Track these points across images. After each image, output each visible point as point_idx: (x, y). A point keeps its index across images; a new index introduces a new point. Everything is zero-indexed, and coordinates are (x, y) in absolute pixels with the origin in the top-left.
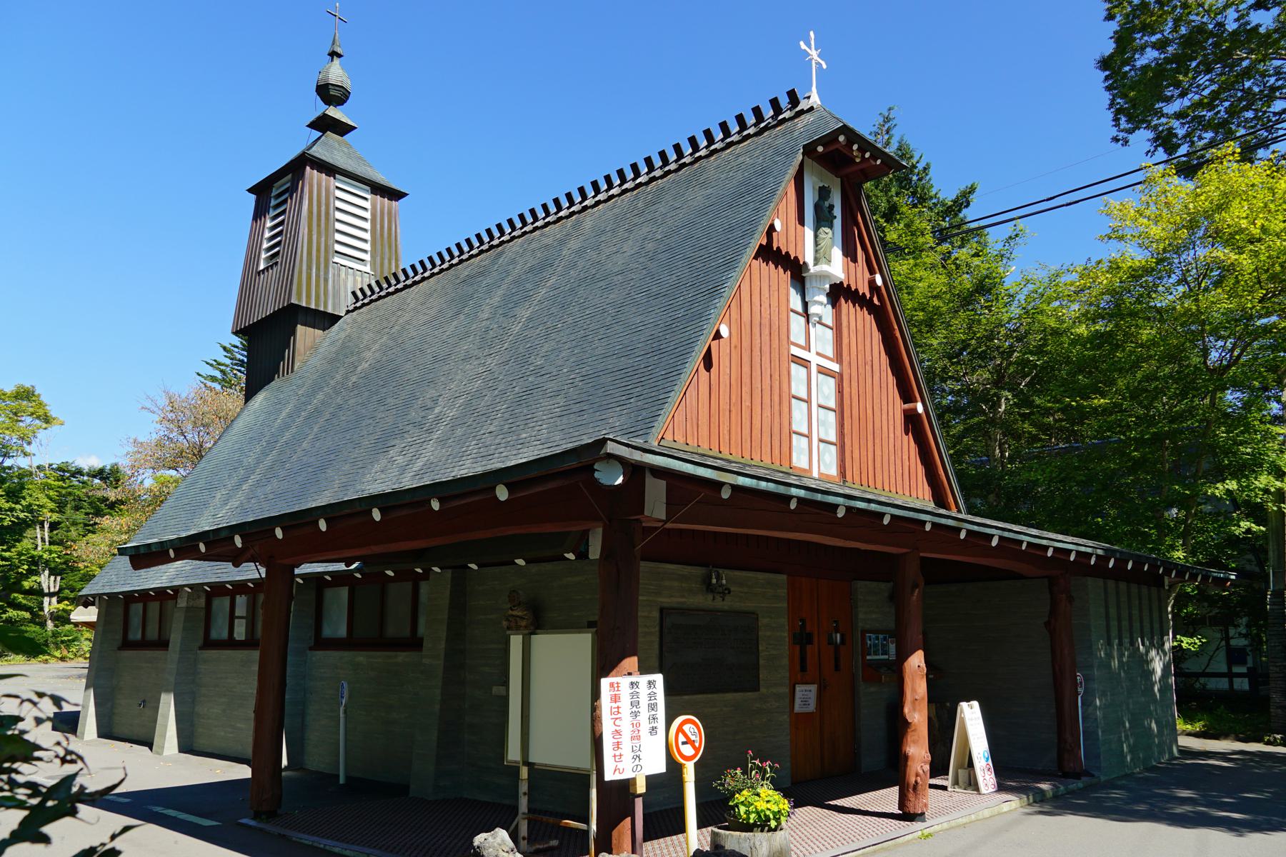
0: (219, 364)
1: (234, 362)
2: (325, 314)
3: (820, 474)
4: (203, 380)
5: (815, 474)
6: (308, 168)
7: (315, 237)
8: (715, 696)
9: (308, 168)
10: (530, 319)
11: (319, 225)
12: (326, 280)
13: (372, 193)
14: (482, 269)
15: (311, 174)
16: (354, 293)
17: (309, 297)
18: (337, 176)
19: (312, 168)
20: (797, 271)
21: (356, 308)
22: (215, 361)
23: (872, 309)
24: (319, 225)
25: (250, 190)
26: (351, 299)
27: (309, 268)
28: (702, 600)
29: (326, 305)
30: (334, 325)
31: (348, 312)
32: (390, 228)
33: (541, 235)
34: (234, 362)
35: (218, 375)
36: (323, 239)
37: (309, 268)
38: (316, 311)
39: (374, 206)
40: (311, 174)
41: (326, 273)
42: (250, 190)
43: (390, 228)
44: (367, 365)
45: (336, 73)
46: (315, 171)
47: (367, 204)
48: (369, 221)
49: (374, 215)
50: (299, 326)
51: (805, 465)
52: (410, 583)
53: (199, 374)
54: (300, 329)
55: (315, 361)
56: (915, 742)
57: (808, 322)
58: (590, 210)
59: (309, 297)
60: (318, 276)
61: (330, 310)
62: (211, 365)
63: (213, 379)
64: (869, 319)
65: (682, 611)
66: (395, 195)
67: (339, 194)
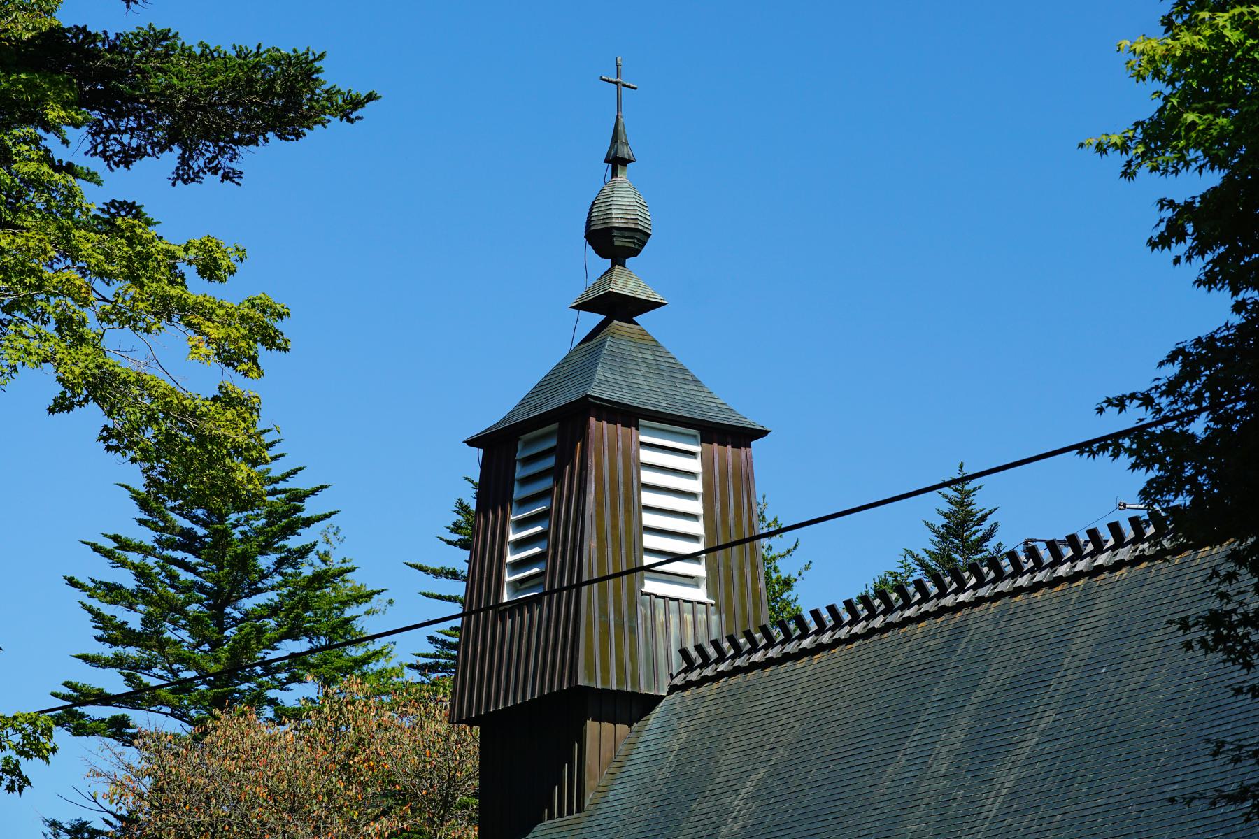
0: (124, 545)
1: (166, 536)
2: (634, 695)
4: (83, 597)
6: (593, 420)
9: (593, 420)
10: (1014, 793)
11: (615, 527)
12: (633, 631)
13: (703, 441)
14: (928, 658)
15: (599, 429)
16: (684, 653)
17: (606, 669)
18: (642, 422)
19: (599, 419)
21: (687, 685)
22: (116, 538)
24: (615, 527)
25: (472, 442)
26: (677, 663)
29: (635, 682)
30: (648, 713)
31: (673, 689)
32: (738, 505)
33: (1030, 607)
34: (166, 536)
35: (128, 580)
37: (604, 613)
38: (620, 694)
39: (707, 465)
40: (599, 429)
41: (633, 616)
42: (472, 442)
43: (738, 505)
44: (737, 827)
46: (605, 423)
47: (695, 465)
48: (701, 520)
49: (708, 485)
50: (589, 722)
53: (72, 582)
54: (591, 725)
55: (621, 793)
58: (1106, 575)
59: (606, 669)
60: (619, 626)
61: (643, 689)
62: (108, 554)
63: (112, 592)
66: (743, 436)
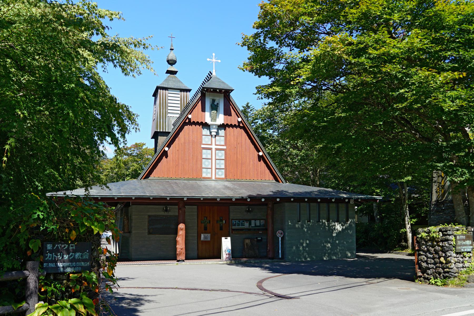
2: (165, 132)
3: (216, 178)
5: (214, 178)
7: (161, 110)
8: (168, 236)
11: (163, 106)
12: (165, 122)
19: (160, 90)
20: (206, 126)
23: (241, 128)
24: (163, 106)
27: (160, 119)
28: (163, 213)
36: (164, 110)
37: (160, 119)
38: (163, 132)
45: (172, 56)
47: (179, 96)
51: (209, 176)
52: (231, 207)
56: (178, 244)
57: (212, 137)
64: (242, 131)
65: (155, 216)
67: (169, 95)
